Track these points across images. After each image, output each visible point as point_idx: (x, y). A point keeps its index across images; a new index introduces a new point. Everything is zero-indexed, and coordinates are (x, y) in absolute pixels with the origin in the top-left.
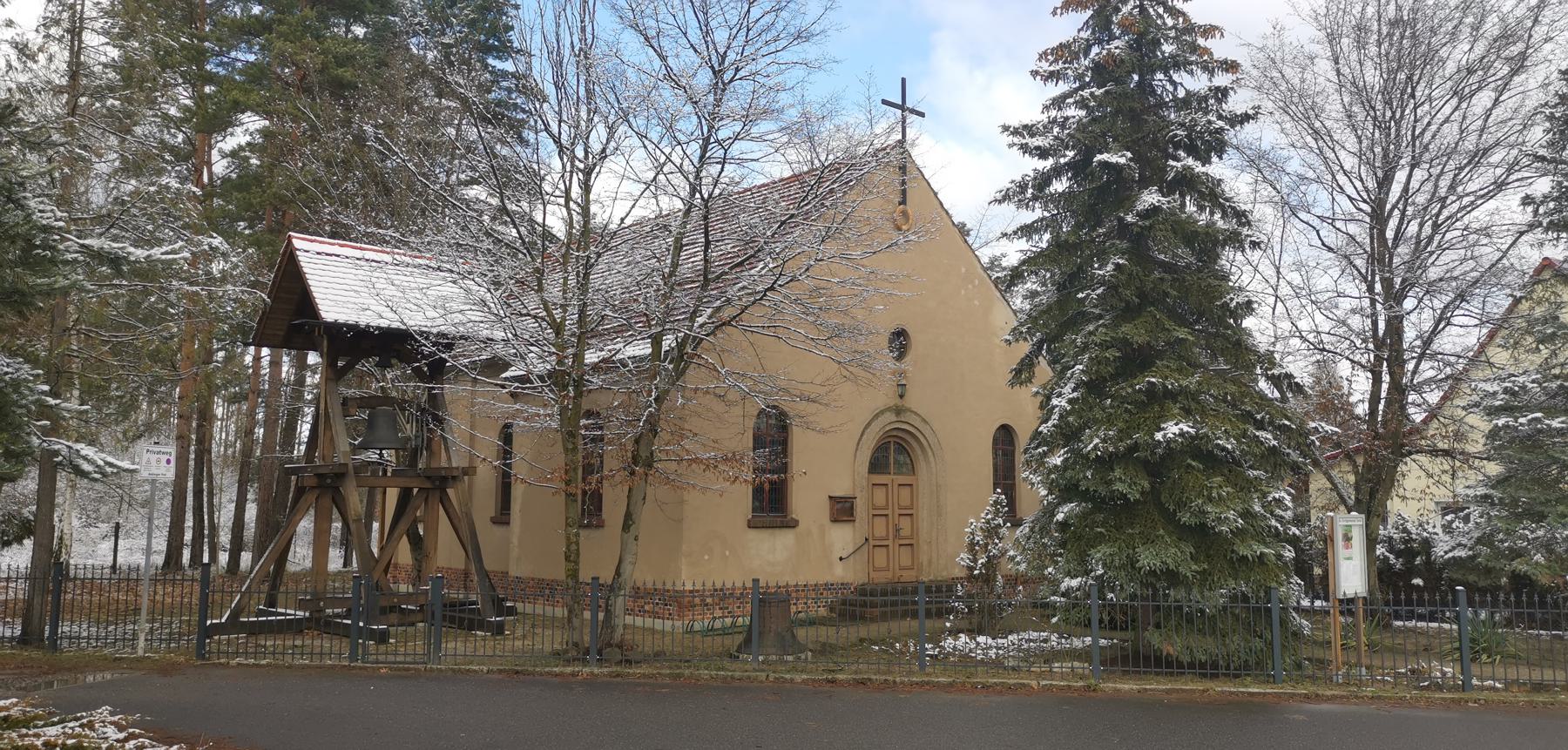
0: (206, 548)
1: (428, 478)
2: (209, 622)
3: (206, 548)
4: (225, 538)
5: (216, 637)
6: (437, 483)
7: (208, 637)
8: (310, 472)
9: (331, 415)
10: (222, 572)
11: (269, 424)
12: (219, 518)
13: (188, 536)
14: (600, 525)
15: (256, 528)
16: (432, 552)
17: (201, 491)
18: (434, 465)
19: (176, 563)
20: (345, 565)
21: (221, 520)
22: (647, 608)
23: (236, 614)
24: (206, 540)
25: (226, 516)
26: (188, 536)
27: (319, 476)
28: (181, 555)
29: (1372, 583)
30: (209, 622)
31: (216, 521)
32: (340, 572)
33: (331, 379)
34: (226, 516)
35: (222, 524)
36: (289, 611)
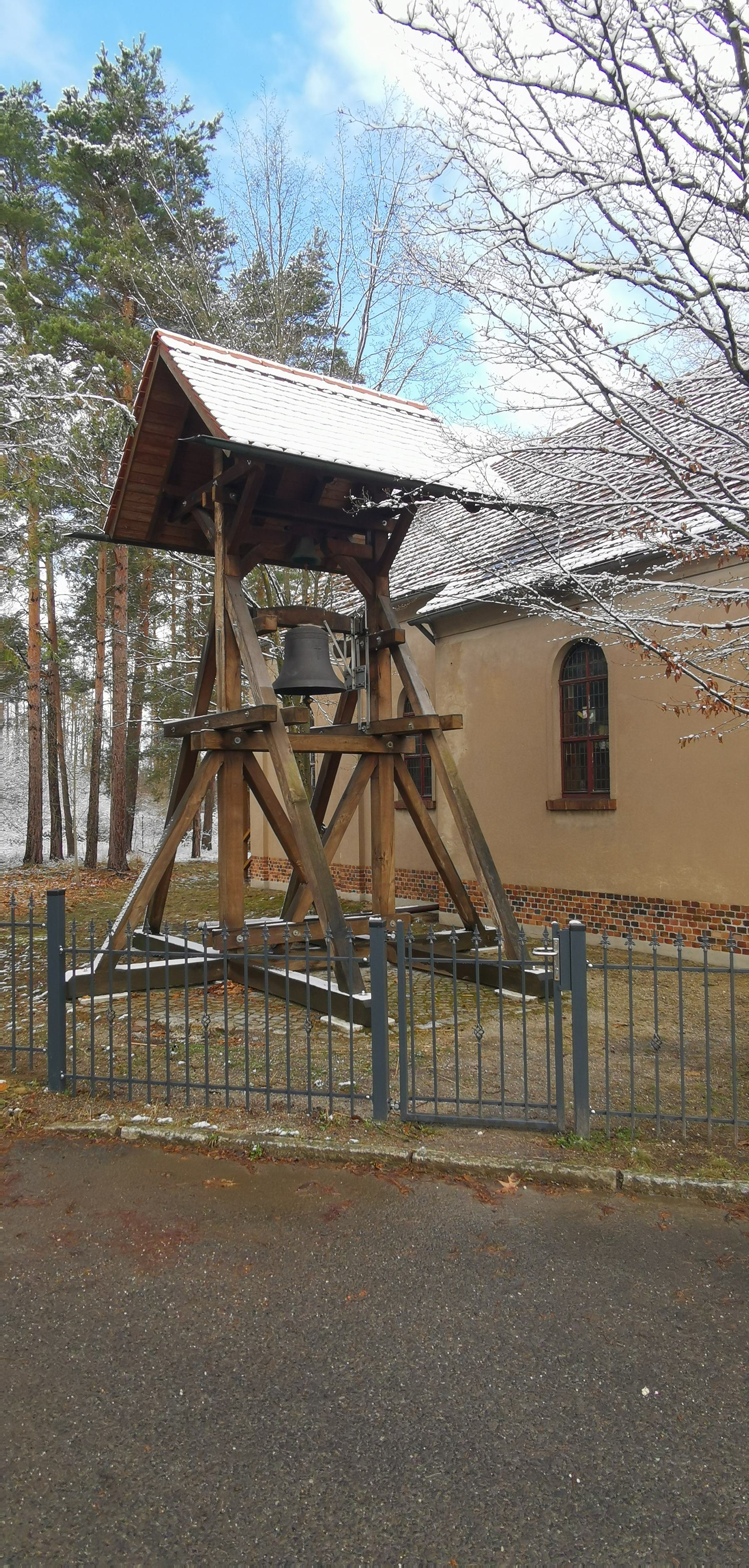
0: (64, 838)
1: (378, 736)
2: (69, 975)
3: (64, 838)
4: (81, 829)
5: (85, 1000)
6: (390, 745)
7: (70, 999)
8: (209, 727)
9: (236, 631)
10: (81, 864)
11: (118, 705)
12: (74, 811)
13: (47, 828)
14: (610, 808)
15: (112, 819)
16: (388, 852)
17: (56, 780)
18: (384, 716)
19: (37, 856)
20: (194, 856)
21: (77, 813)
22: (716, 934)
23: (112, 957)
24: (64, 831)
25: (80, 808)
26: (47, 828)
27: (223, 731)
28: (40, 847)
29: (336, 839)
30: (69, 975)
31: (72, 815)
32: (190, 862)
33: (230, 576)
34: (80, 808)
35: (77, 816)
36: (192, 945)
